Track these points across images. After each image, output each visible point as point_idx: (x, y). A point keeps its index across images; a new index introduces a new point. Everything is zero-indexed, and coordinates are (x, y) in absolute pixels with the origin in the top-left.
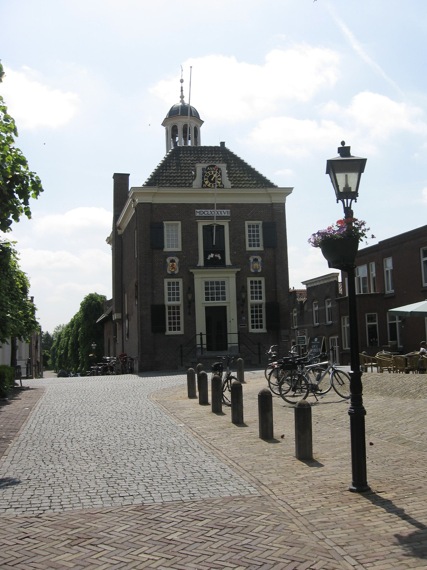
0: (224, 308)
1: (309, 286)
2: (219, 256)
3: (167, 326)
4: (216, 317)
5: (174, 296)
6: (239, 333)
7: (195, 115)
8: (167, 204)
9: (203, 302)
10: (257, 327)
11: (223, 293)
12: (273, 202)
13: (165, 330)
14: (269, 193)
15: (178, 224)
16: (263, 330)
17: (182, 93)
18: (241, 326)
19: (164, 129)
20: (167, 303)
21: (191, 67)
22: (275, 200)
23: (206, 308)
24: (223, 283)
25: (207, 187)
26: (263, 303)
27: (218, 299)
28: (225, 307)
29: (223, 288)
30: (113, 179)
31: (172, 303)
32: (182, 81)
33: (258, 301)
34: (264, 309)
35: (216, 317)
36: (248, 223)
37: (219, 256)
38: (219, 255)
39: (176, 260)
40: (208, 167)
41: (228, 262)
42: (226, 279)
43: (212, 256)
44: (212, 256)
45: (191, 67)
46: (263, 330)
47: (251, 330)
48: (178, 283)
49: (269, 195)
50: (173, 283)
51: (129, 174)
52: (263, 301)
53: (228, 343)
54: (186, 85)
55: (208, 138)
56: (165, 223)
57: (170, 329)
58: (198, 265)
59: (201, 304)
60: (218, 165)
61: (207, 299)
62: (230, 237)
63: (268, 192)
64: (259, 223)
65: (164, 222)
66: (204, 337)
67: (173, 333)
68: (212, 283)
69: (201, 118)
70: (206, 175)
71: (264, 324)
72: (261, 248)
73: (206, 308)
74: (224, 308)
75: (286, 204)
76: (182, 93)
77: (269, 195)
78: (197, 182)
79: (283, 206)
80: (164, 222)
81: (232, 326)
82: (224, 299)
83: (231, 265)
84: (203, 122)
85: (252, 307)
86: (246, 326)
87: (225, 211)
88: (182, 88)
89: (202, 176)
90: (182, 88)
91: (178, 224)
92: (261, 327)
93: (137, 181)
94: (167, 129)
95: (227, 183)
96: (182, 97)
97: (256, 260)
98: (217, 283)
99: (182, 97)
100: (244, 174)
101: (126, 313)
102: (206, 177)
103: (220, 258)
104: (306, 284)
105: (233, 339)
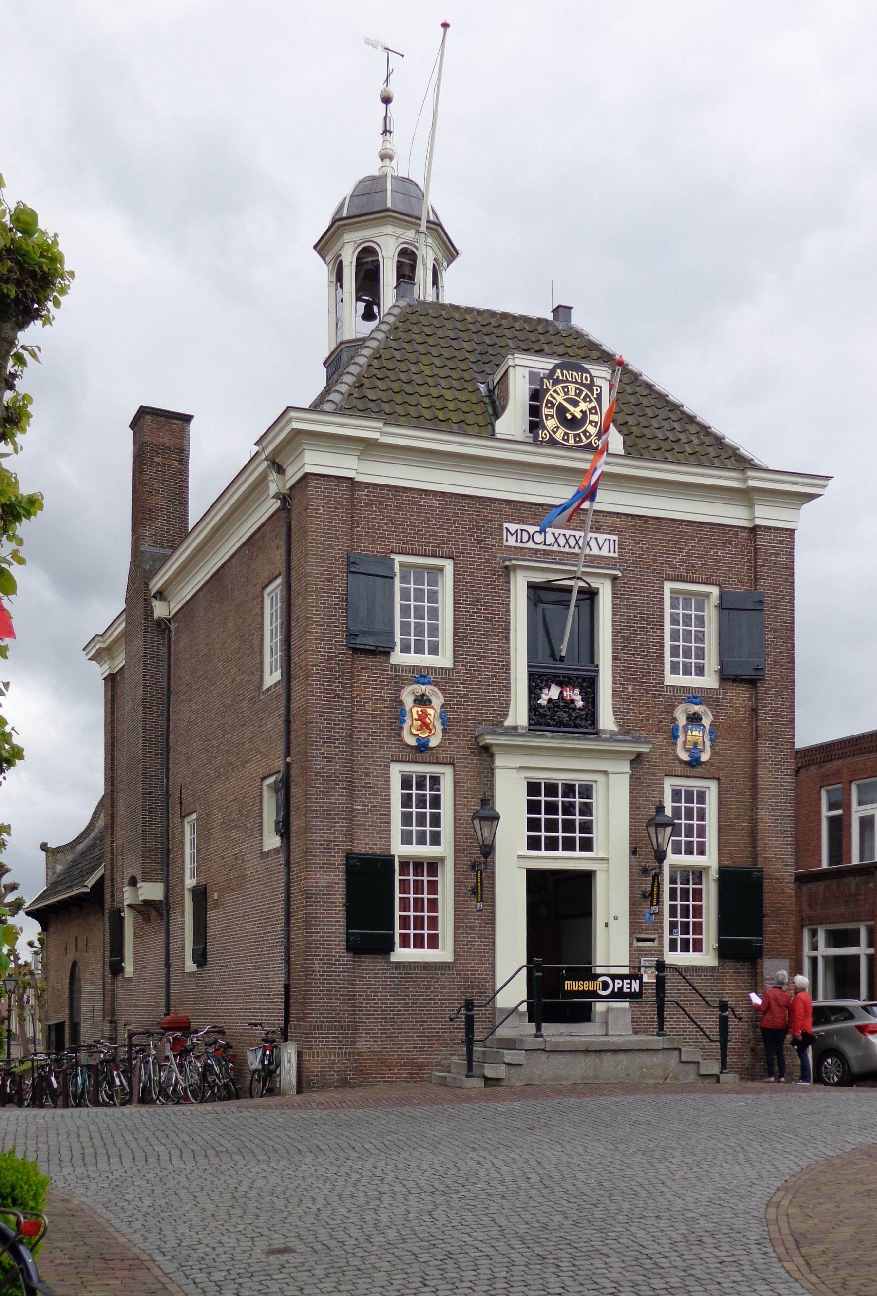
0: (586, 879)
2: (575, 696)
8: (406, 489)
11: (587, 827)
12: (758, 522)
18: (639, 940)
21: (445, 26)
22: (768, 515)
24: (587, 791)
25: (552, 442)
29: (587, 810)
37: (575, 696)
38: (577, 691)
39: (433, 699)
41: (607, 720)
42: (600, 778)
43: (554, 692)
44: (554, 692)
52: (710, 860)
57: (405, 649)
58: (508, 723)
59: (514, 859)
61: (534, 843)
63: (752, 483)
65: (392, 556)
68: (551, 789)
72: (709, 681)
77: (747, 496)
78: (512, 421)
80: (392, 556)
81: (612, 944)
82: (587, 845)
83: (616, 729)
86: (656, 944)
87: (601, 537)
91: (441, 569)
97: (694, 719)
98: (569, 789)
103: (580, 704)
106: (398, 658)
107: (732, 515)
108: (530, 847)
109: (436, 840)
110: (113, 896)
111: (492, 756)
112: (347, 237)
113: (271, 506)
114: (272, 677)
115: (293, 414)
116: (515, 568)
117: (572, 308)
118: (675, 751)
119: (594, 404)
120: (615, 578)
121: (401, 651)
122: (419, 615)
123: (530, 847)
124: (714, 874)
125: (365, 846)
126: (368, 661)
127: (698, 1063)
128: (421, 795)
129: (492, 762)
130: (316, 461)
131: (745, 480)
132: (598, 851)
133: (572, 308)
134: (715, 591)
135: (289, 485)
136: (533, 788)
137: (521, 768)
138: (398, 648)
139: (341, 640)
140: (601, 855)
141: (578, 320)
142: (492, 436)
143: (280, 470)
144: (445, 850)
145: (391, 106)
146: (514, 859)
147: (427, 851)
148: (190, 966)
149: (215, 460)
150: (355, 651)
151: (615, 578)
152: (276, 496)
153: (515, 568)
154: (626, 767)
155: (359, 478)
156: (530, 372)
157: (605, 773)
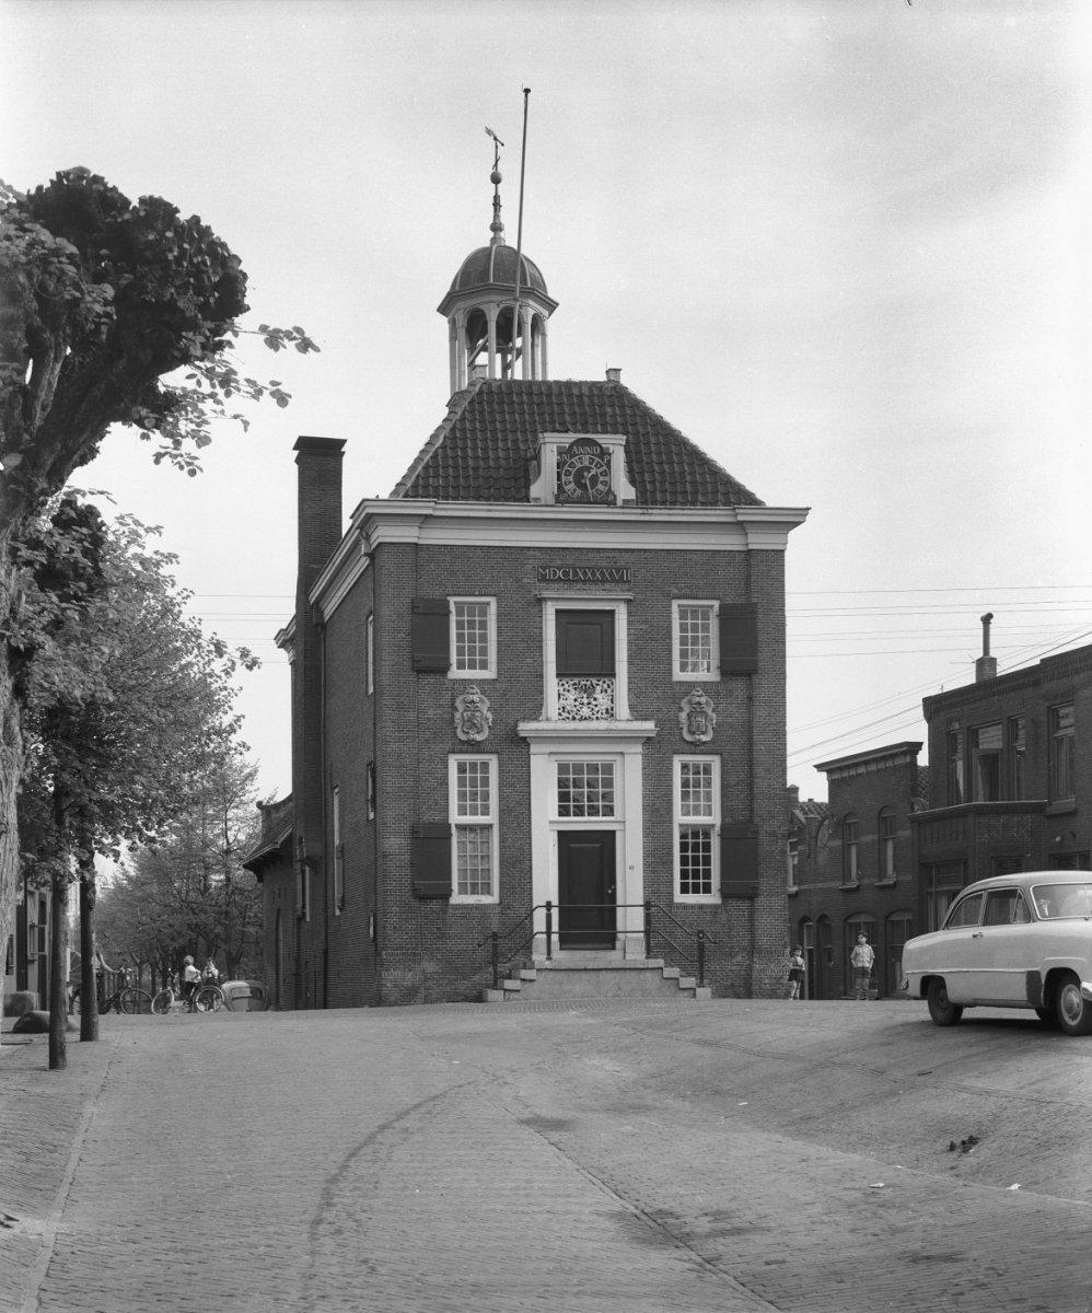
0: (609, 837)
1: (836, 776)
3: (454, 658)
4: (588, 861)
5: (474, 797)
6: (647, 905)
7: (534, 289)
9: (552, 819)
10: (696, 890)
11: (608, 796)
12: (751, 547)
13: (445, 669)
14: (742, 523)
15: (488, 604)
16: (713, 898)
17: (496, 216)
19: (443, 322)
20: (455, 818)
22: (758, 541)
23: (561, 834)
24: (608, 768)
26: (713, 826)
27: (594, 811)
28: (614, 832)
29: (609, 783)
30: (297, 466)
31: (468, 819)
32: (496, 179)
33: (701, 819)
34: (715, 843)
35: (588, 861)
36: (679, 606)
40: (572, 445)
42: (618, 758)
45: (527, 91)
46: (713, 898)
47: (679, 898)
48: (484, 665)
49: (741, 527)
50: (474, 766)
51: (342, 442)
52: (715, 819)
53: (619, 929)
54: (508, 191)
55: (569, 354)
56: (452, 600)
57: (461, 666)
59: (546, 820)
60: (605, 440)
61: (564, 811)
62: (630, 643)
63: (740, 518)
64: (712, 607)
65: (449, 598)
66: (555, 912)
67: (470, 899)
68: (578, 768)
69: (552, 294)
70: (566, 468)
71: (715, 881)
73: (561, 834)
74: (609, 837)
75: (787, 555)
76: (496, 216)
77: (741, 527)
78: (543, 486)
79: (779, 554)
80: (449, 598)
81: (631, 884)
82: (609, 811)
84: (557, 304)
85: (683, 836)
88: (496, 198)
89: (555, 469)
90: (496, 198)
91: (488, 604)
92: (707, 889)
93: (369, 478)
94: (453, 323)
95: (624, 489)
96: (496, 227)
98: (593, 768)
99: (496, 227)
100: (675, 470)
101: (337, 842)
102: (568, 473)
104: (829, 772)
105: (630, 919)
106: (455, 673)
107: (729, 542)
108: (560, 814)
109: (486, 812)
110: (625, 891)
111: (529, 745)
112: (458, 305)
113: (364, 562)
114: (371, 690)
115: (366, 503)
116: (546, 599)
117: (620, 370)
118: (681, 733)
119: (605, 468)
120: (628, 601)
121: (458, 668)
122: (471, 640)
123: (560, 814)
124: (717, 829)
125: (429, 817)
126: (431, 679)
127: (662, 969)
128: (473, 780)
129: (529, 748)
130: (384, 534)
131: (736, 515)
132: (618, 815)
133: (620, 370)
134: (716, 604)
135: (373, 547)
136: (563, 768)
137: (551, 753)
138: (454, 666)
139: (408, 664)
140: (619, 819)
141: (625, 380)
142: (527, 499)
143: (368, 538)
144: (492, 818)
145: (499, 185)
146: (546, 820)
147: (480, 819)
148: (338, 912)
149: (369, 478)
150: (419, 672)
151: (628, 601)
152: (366, 554)
153: (546, 599)
154: (639, 748)
155: (420, 542)
156: (558, 447)
157: (622, 753)
